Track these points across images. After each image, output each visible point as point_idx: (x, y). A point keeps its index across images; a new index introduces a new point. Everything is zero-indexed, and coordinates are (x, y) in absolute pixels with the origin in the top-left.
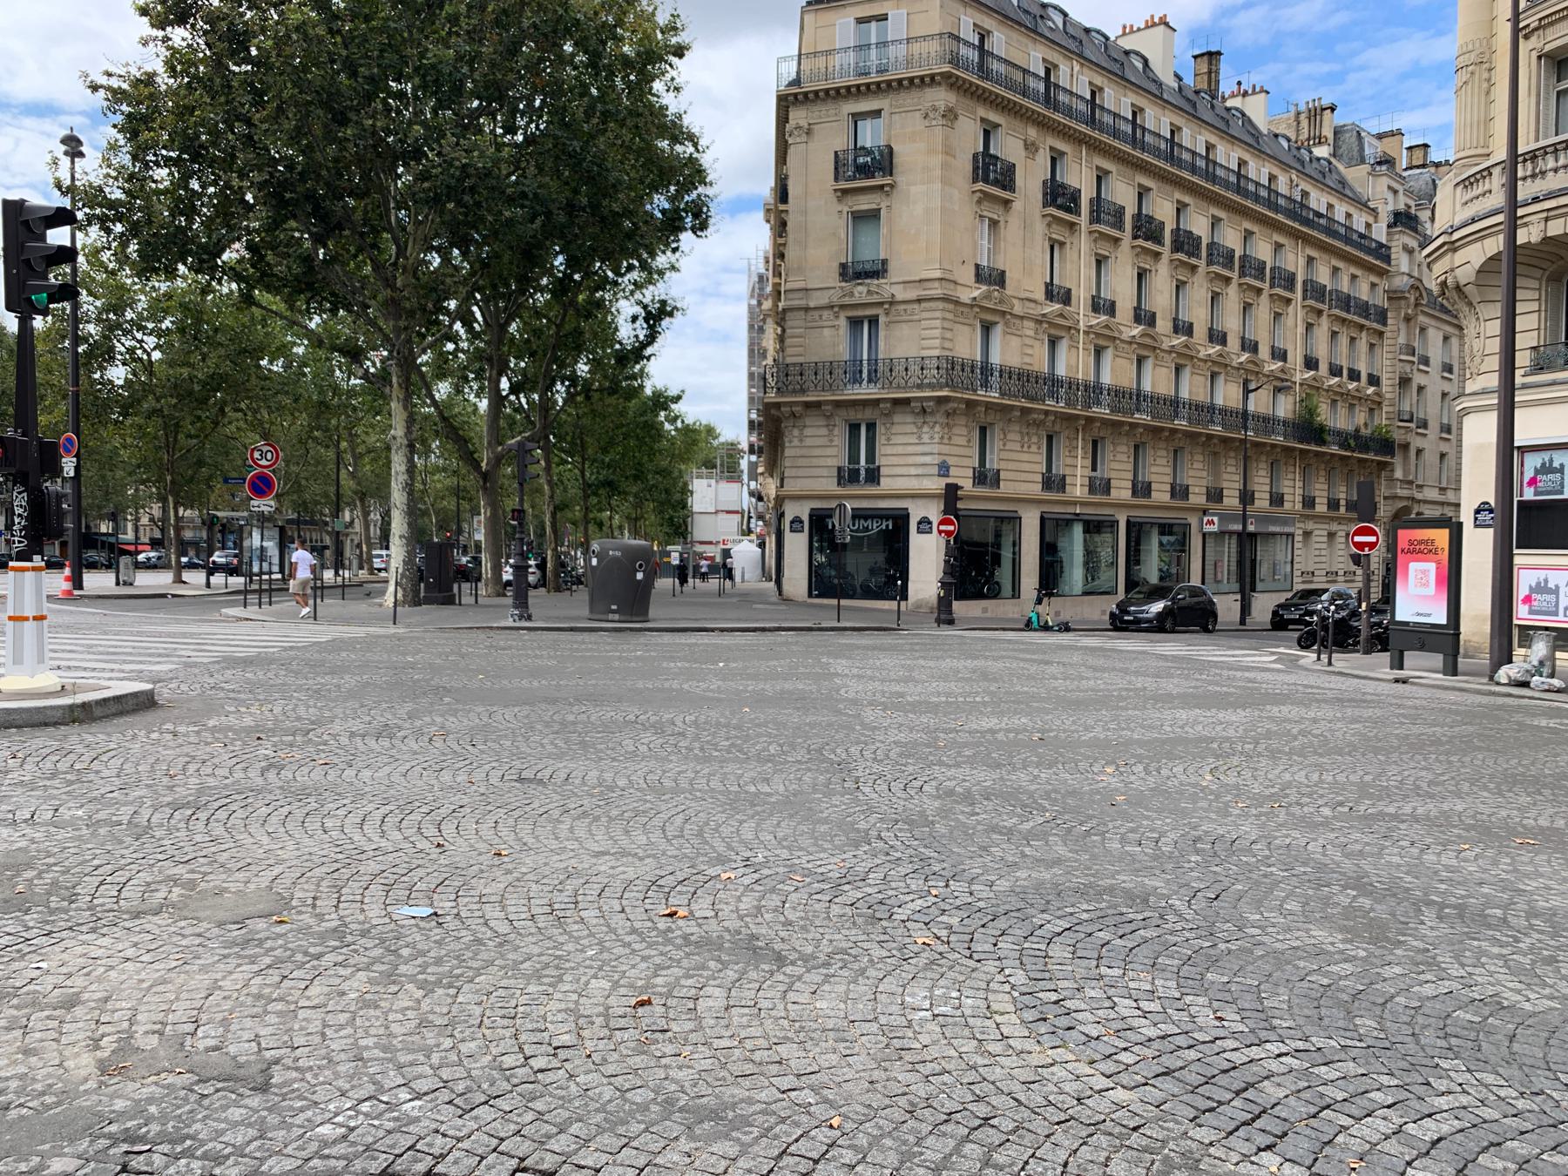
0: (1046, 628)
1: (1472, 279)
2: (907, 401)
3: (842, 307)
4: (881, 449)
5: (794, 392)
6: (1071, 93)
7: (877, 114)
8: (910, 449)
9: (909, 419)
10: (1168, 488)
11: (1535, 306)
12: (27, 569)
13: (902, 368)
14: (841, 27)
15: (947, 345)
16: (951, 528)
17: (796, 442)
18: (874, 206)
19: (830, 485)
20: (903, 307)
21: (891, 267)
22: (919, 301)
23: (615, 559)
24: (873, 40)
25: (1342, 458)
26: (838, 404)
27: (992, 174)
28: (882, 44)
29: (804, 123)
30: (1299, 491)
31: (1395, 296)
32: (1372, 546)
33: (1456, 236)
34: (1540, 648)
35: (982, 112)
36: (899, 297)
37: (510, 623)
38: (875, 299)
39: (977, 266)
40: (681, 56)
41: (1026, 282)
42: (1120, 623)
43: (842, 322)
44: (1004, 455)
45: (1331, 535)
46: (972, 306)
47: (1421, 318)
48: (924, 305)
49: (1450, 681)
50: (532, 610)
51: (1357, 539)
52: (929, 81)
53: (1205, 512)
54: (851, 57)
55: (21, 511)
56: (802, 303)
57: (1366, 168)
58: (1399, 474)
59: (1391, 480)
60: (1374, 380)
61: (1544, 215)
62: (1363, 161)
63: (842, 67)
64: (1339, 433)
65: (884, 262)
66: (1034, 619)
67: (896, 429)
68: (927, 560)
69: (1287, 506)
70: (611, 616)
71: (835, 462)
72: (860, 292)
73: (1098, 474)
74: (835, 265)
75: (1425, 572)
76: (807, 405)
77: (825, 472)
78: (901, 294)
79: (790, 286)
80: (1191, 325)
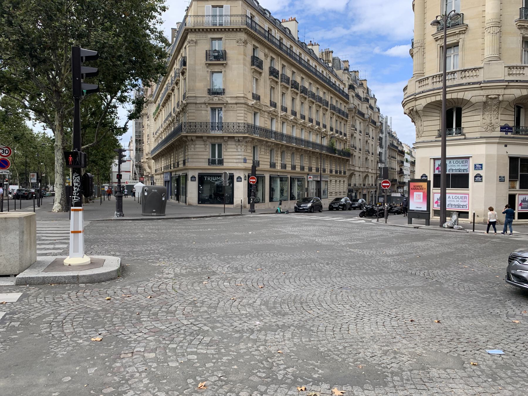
0: (283, 213)
1: (422, 109)
2: (233, 137)
3: (209, 104)
5: (193, 132)
7: (220, 39)
9: (234, 143)
10: (269, 164)
11: (438, 118)
12: (80, 210)
13: (226, 126)
14: (207, 8)
15: (246, 119)
16: (254, 180)
17: (193, 150)
19: (205, 165)
20: (230, 105)
21: (226, 91)
22: (236, 104)
23: (155, 193)
24: (218, 14)
25: (339, 158)
27: (256, 62)
28: (221, 16)
29: (194, 39)
30: (329, 168)
31: (350, 110)
32: (388, 186)
33: (417, 96)
34: (455, 217)
35: (254, 43)
36: (229, 102)
37: (115, 217)
38: (221, 102)
39: (253, 93)
40: (165, 11)
41: (265, 100)
42: (297, 210)
43: (209, 109)
44: (261, 156)
45: (336, 181)
46: (252, 107)
47: (356, 117)
48: (238, 105)
49: (428, 227)
50: (124, 213)
51: (384, 184)
52: (239, 30)
53: (308, 175)
54: (210, 19)
55: (77, 184)
56: (195, 101)
57: (342, 71)
58: (351, 163)
59: (349, 164)
60: (345, 135)
62: (340, 69)
63: (207, 22)
64: (338, 151)
66: (279, 210)
67: (229, 146)
68: (240, 192)
69: (326, 172)
70: (153, 214)
71: (207, 157)
72: (216, 99)
73: (283, 162)
74: (206, 89)
75: (419, 195)
76: (197, 137)
77: (204, 160)
79: (189, 95)
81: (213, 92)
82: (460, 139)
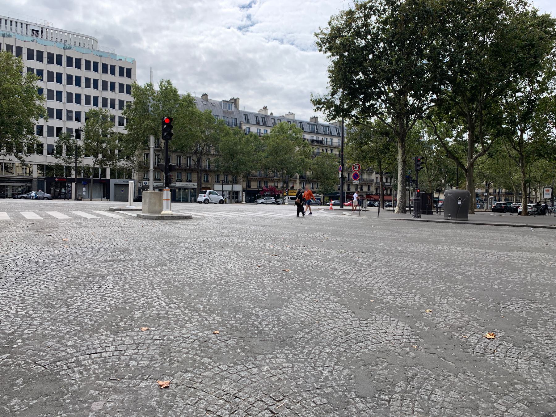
70: (449, 218)
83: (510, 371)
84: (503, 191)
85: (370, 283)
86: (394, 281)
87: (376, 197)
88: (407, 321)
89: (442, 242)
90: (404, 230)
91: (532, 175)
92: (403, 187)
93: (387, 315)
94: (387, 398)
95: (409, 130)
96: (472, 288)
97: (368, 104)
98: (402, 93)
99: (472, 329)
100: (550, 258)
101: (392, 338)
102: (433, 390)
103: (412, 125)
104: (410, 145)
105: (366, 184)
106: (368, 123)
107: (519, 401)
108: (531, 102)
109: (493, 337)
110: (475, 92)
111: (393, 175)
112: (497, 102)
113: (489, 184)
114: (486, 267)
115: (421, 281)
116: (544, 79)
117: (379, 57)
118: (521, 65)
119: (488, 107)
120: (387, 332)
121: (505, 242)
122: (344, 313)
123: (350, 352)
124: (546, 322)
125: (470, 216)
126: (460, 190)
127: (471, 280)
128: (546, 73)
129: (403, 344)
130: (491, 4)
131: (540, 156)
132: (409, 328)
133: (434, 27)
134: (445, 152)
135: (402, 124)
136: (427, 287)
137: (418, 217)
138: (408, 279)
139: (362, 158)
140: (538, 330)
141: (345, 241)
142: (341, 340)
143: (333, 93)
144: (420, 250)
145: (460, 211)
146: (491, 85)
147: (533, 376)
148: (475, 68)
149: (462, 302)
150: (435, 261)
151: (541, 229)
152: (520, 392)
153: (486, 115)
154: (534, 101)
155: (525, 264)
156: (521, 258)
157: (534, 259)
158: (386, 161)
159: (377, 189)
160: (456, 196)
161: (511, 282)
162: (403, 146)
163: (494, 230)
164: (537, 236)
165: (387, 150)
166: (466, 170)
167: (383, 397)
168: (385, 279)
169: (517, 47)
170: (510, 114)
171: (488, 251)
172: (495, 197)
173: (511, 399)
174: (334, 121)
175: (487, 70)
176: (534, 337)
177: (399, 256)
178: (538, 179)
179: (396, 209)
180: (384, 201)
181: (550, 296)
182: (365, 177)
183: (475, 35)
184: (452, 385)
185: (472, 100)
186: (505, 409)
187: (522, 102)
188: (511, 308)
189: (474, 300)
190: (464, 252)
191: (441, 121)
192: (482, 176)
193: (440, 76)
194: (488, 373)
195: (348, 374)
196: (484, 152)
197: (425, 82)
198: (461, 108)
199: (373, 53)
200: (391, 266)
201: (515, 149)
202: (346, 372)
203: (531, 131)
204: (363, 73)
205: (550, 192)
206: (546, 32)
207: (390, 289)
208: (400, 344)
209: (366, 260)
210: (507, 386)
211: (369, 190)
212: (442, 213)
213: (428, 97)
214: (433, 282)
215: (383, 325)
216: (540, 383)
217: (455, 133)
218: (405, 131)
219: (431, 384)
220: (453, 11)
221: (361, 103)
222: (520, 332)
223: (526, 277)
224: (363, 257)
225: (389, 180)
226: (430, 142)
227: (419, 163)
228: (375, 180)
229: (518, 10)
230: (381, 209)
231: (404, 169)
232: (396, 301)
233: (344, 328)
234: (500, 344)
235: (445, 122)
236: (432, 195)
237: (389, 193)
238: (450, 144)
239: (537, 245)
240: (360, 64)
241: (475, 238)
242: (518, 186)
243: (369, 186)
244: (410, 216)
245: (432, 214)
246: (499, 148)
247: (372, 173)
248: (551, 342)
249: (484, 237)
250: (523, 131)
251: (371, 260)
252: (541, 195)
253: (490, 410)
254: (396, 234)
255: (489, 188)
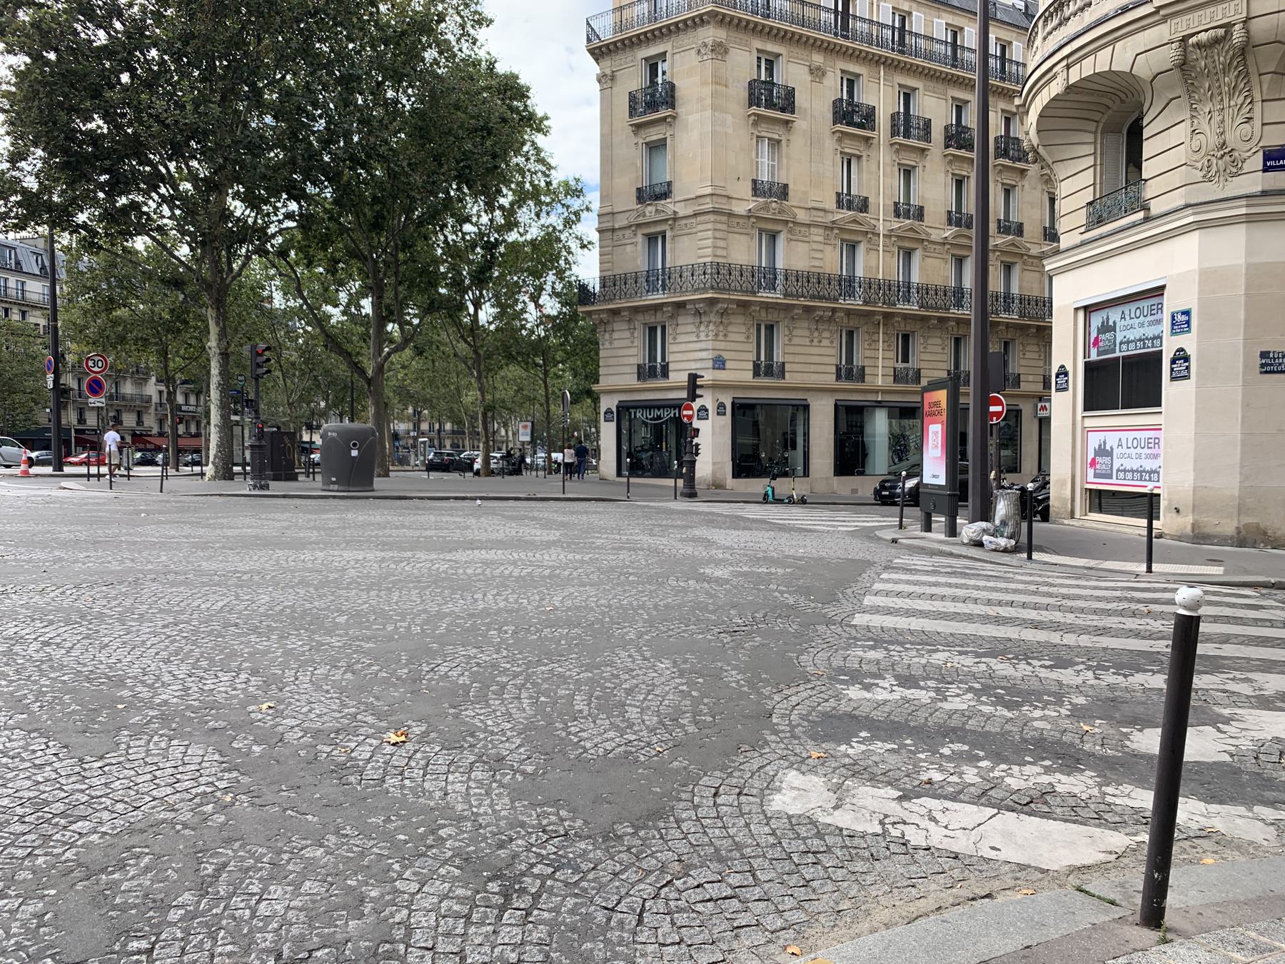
0: (779, 501)
3: (639, 226)
4: (670, 348)
6: (871, 21)
8: (692, 346)
15: (719, 252)
17: (607, 345)
18: (661, 136)
19: (631, 380)
20: (684, 222)
21: (676, 188)
22: (695, 215)
23: (333, 438)
26: (636, 310)
27: (770, 99)
36: (681, 214)
43: (640, 238)
48: (700, 219)
61: (1064, 63)
65: (669, 184)
68: (713, 443)
70: (332, 487)
71: (634, 361)
74: (1041, 230)
77: (628, 369)
78: (682, 210)
80: (1021, 225)
81: (845, 201)
82: (1134, 225)
83: (432, 804)
84: (448, 426)
85: (120, 661)
86: (187, 649)
87: (158, 441)
88: (213, 739)
89: (311, 543)
90: (224, 521)
91: (497, 396)
92: (225, 418)
93: (161, 736)
94: (144, 945)
95: (234, 278)
96: (369, 639)
97: (123, 201)
98: (213, 187)
99: (362, 731)
100: (520, 559)
101: (169, 790)
102: (264, 890)
103: (241, 269)
104: (239, 315)
105: (130, 409)
106: (124, 249)
107: (445, 862)
108: (490, 247)
109: (403, 738)
110: (382, 209)
111: (200, 389)
112: (426, 238)
113: (420, 413)
114: (400, 590)
115: (253, 638)
116: (512, 204)
117: (150, 82)
118: (469, 167)
119: (410, 247)
120: (156, 778)
121: (444, 533)
122: (34, 752)
123: (46, 855)
124: (503, 686)
125: (378, 482)
126: (357, 425)
127: (368, 621)
128: (514, 192)
129: (197, 800)
130: (408, 24)
131: (510, 358)
132: (216, 757)
133: (288, 41)
134: (321, 338)
135: (216, 262)
136: (265, 653)
137: (262, 488)
138: (223, 637)
139: (113, 339)
140: (489, 706)
141: (59, 560)
142: (19, 828)
143: (16, 158)
144: (257, 566)
145: (357, 472)
146: (413, 200)
147: (474, 803)
148: (379, 155)
149: (345, 672)
150: (292, 587)
151: (511, 503)
152: (449, 844)
153: (405, 262)
154: (497, 244)
155: (475, 575)
156: (469, 563)
157: (493, 562)
158: (182, 352)
159: (161, 422)
160: (348, 438)
161: (447, 615)
162: (222, 317)
163: (424, 509)
164: (503, 516)
165: (179, 322)
166: (369, 382)
167: (135, 945)
168: (162, 646)
169: (461, 127)
170: (453, 268)
171: (409, 554)
172: (431, 440)
173: (430, 861)
174: (24, 234)
175: (405, 164)
176: (482, 721)
177: (204, 584)
178: (509, 405)
179: (209, 470)
180: (179, 451)
181: (515, 632)
182: (128, 388)
183: (379, 84)
184: (310, 867)
185: (377, 225)
186: (418, 886)
187: (473, 245)
188: (443, 669)
189: (370, 665)
190: (357, 561)
191: (309, 265)
192: (406, 396)
193: (304, 159)
194: (388, 820)
195: (35, 915)
196: (406, 341)
197: (267, 167)
198: (353, 241)
199: (132, 71)
200: (182, 612)
201: (466, 341)
202: (31, 909)
203: (493, 306)
204: (103, 118)
205: (529, 431)
206: (511, 108)
207: (173, 668)
208: (191, 800)
209: (114, 603)
210: (423, 837)
211: (140, 422)
212: (319, 477)
213: (279, 205)
214: (281, 637)
215: (146, 763)
216: (486, 813)
217: (343, 297)
218: (223, 280)
219: (260, 879)
220: (327, 15)
221: (101, 195)
222: (456, 716)
223: (476, 600)
224: (105, 597)
225: (192, 400)
226: (288, 313)
227: (260, 359)
228: (155, 399)
229: (460, 50)
230: (171, 471)
231: (224, 373)
232: (188, 695)
233: (31, 794)
234: (416, 752)
235: (321, 270)
236: (293, 436)
237: (193, 430)
238: (333, 321)
239: (501, 536)
240: (96, 94)
241: (385, 528)
242: (474, 418)
243: (139, 414)
244: (243, 486)
245: (296, 479)
246: (435, 337)
247: (146, 380)
248: (509, 726)
249: (403, 526)
250: (477, 305)
251: (128, 603)
252: (514, 434)
253: (387, 898)
254: (202, 531)
255: (419, 421)
